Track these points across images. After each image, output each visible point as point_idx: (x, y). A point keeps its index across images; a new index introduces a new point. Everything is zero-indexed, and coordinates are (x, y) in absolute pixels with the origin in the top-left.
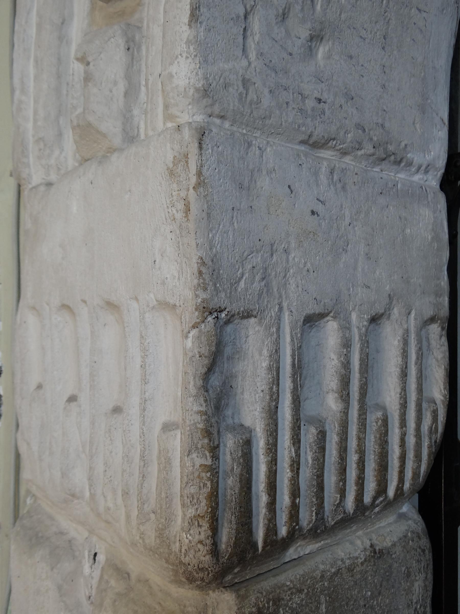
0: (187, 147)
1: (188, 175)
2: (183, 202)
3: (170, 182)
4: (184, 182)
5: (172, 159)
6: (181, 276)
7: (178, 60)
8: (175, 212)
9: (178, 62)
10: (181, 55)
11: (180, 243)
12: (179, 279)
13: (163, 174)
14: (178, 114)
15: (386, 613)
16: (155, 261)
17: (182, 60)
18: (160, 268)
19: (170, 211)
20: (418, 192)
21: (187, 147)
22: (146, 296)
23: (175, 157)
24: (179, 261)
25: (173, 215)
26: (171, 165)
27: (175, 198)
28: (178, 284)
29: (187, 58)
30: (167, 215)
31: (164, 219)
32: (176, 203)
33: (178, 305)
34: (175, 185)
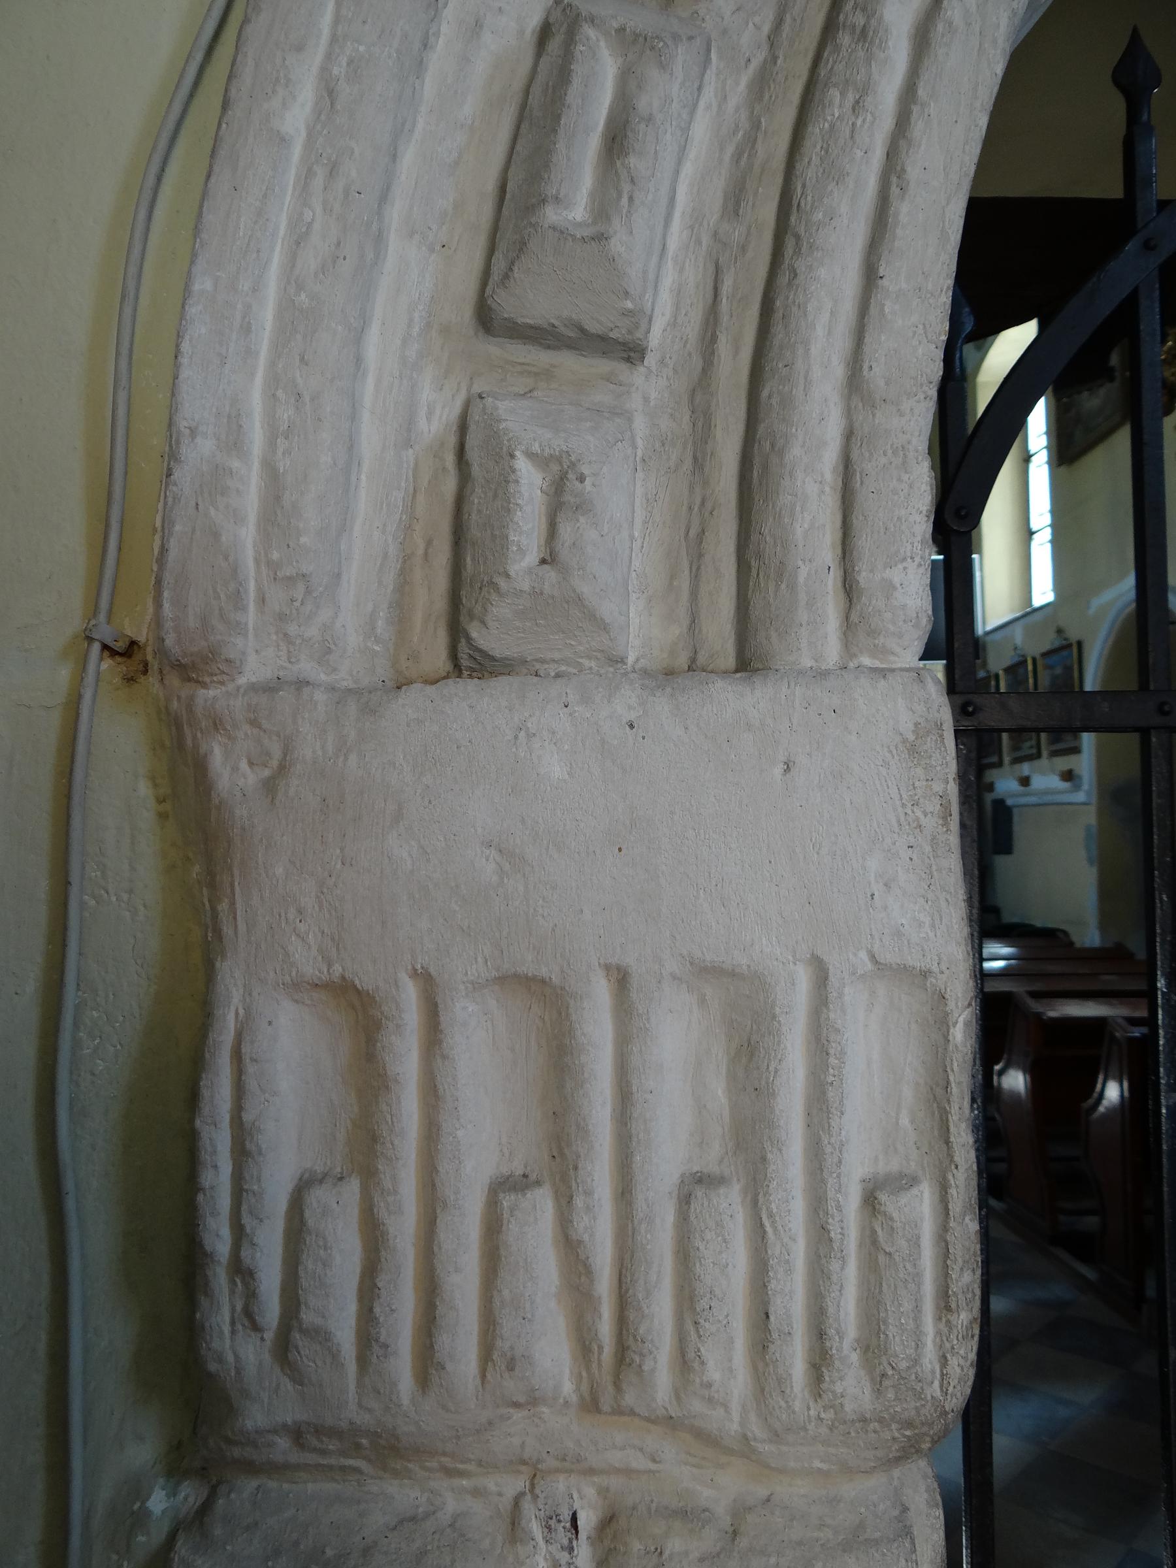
0: (938, 711)
1: (944, 758)
2: (937, 801)
3: (910, 764)
4: (938, 768)
5: (911, 726)
6: (937, 922)
7: (905, 564)
8: (919, 813)
9: (905, 568)
10: (912, 558)
11: (934, 868)
12: (933, 926)
13: (893, 749)
14: (898, 650)
15: (584, 1553)
16: (873, 895)
17: (912, 566)
18: (885, 908)
19: (909, 812)
20: (161, 694)
21: (938, 711)
22: (851, 956)
23: (916, 724)
24: (930, 896)
25: (917, 819)
26: (911, 737)
27: (919, 791)
28: (931, 935)
29: (920, 565)
30: (902, 818)
31: (896, 825)
32: (922, 800)
33: (935, 968)
34: (919, 771)
